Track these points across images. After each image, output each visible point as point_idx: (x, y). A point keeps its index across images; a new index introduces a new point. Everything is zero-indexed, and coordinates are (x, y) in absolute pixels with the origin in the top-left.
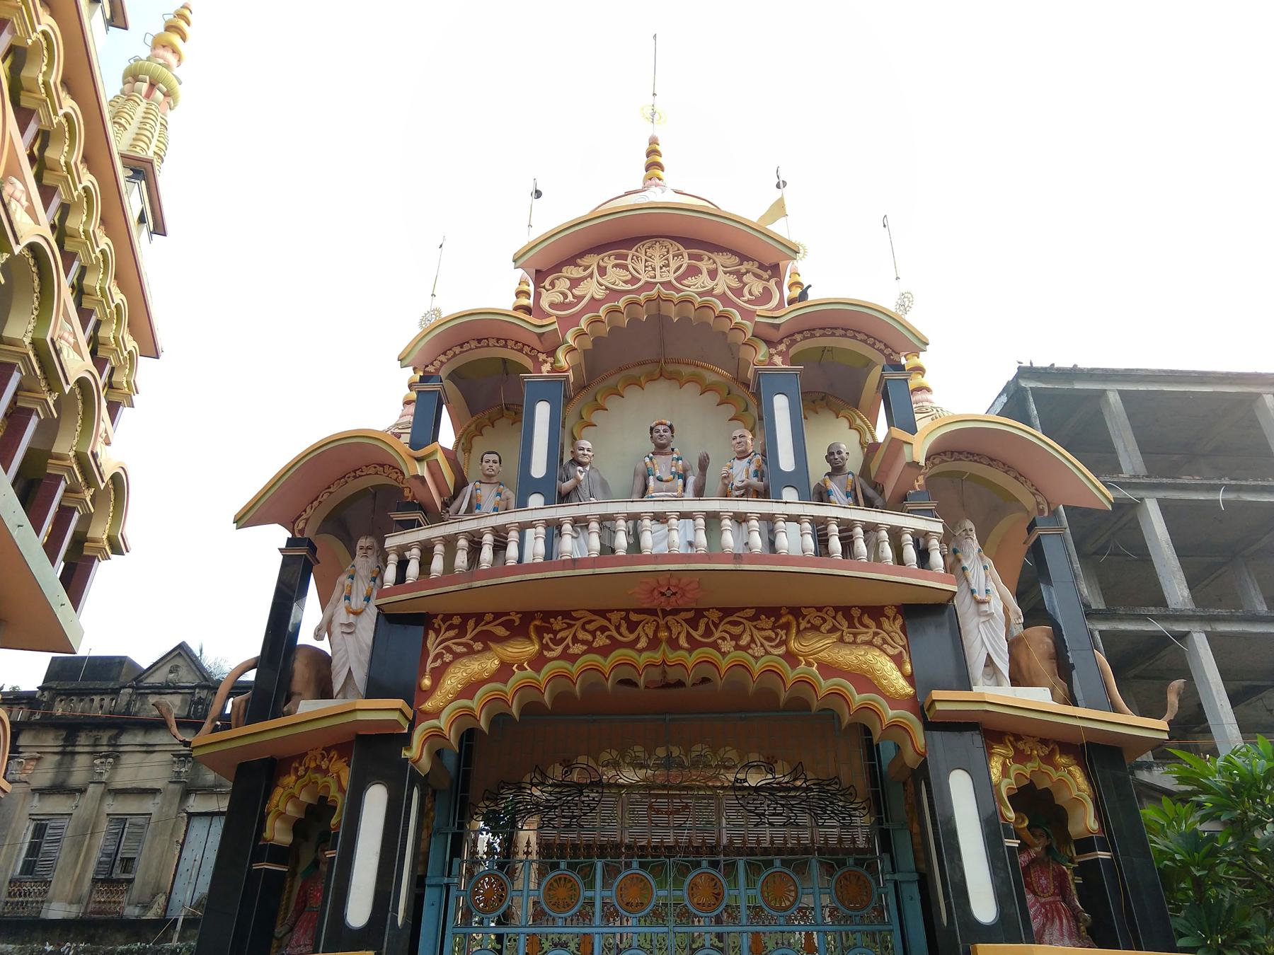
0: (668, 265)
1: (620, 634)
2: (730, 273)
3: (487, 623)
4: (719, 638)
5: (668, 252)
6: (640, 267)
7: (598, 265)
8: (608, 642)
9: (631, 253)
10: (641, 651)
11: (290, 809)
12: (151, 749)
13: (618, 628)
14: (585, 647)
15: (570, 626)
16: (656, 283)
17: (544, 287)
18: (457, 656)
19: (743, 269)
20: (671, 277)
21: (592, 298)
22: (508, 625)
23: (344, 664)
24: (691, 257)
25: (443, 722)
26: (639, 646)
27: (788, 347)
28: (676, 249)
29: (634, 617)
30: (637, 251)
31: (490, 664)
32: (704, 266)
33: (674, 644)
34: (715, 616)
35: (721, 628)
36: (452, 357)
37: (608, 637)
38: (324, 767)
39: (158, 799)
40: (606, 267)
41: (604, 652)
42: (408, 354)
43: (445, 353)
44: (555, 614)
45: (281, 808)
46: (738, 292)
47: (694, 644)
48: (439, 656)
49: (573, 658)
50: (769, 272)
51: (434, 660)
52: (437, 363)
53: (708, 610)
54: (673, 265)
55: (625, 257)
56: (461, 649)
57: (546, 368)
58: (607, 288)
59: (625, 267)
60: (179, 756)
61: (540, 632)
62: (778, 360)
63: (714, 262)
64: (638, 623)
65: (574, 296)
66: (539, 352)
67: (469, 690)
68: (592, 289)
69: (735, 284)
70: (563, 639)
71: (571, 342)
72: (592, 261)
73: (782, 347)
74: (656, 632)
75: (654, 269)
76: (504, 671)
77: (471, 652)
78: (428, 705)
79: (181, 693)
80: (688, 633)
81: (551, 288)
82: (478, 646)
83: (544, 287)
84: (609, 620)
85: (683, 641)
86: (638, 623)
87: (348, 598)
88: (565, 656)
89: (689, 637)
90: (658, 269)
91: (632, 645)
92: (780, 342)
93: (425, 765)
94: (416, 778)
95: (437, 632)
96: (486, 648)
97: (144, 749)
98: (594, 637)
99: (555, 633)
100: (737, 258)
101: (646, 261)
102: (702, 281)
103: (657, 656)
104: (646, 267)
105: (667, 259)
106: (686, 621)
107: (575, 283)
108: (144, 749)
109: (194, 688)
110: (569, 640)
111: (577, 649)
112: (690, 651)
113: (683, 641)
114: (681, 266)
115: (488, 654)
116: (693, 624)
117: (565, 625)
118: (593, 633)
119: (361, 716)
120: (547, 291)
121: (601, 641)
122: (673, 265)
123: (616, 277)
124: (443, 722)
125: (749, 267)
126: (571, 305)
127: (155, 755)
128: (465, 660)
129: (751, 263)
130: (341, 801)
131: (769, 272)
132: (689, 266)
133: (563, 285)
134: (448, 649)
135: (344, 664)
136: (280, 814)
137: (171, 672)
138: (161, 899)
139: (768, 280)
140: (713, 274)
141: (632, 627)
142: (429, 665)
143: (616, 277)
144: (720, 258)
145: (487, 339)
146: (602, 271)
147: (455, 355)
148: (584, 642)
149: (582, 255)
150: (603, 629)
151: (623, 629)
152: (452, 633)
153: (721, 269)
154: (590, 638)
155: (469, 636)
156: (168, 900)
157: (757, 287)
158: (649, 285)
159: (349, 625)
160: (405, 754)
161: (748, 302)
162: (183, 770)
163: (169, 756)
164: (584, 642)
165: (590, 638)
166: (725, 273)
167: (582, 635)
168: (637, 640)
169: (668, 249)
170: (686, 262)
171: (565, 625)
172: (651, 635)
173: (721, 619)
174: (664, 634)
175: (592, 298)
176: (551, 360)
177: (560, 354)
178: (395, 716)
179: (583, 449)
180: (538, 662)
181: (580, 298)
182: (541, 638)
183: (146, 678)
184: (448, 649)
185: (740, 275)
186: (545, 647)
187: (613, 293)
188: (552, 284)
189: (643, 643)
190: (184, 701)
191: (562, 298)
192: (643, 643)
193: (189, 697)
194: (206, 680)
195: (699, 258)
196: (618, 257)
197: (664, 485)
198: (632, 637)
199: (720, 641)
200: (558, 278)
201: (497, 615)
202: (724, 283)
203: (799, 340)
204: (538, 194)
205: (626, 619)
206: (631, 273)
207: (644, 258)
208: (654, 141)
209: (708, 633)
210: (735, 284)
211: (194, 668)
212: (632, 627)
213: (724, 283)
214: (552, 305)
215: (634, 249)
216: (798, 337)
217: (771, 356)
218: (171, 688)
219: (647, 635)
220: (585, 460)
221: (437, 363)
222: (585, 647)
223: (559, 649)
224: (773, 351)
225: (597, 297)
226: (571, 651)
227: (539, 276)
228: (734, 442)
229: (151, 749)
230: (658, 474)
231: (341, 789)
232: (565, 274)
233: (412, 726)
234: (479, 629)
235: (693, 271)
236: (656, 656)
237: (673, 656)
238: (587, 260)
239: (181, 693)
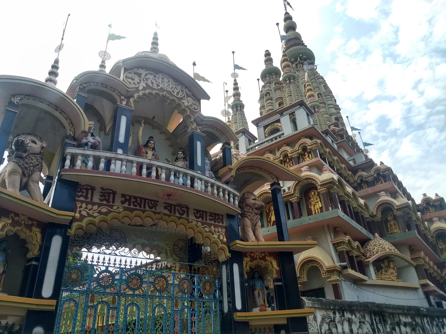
27: (202, 128)
62: (199, 130)
92: (201, 125)
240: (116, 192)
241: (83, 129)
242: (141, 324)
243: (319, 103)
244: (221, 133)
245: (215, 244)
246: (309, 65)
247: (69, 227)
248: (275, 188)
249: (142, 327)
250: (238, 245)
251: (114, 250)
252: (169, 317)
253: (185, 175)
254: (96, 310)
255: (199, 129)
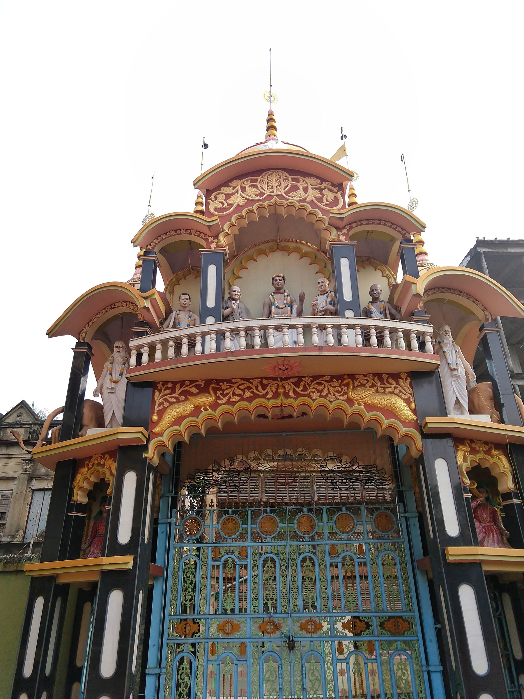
0: (280, 185)
1: (258, 391)
2: (316, 189)
3: (186, 386)
4: (311, 392)
5: (280, 178)
6: (265, 186)
7: (241, 186)
8: (251, 395)
9: (259, 178)
10: (269, 399)
11: (85, 485)
12: (10, 456)
13: (256, 388)
14: (239, 398)
15: (231, 387)
16: (274, 195)
17: (211, 199)
18: (171, 404)
19: (322, 186)
20: (282, 192)
21: (238, 205)
22: (196, 387)
23: (111, 409)
24: (293, 180)
25: (165, 438)
26: (268, 397)
27: (348, 231)
28: (285, 175)
29: (265, 382)
30: (262, 177)
31: (188, 407)
32: (301, 185)
33: (287, 395)
34: (308, 380)
35: (312, 387)
36: (161, 240)
37: (252, 392)
38: (102, 463)
39: (16, 482)
40: (245, 187)
41: (250, 400)
42: (137, 239)
43: (157, 238)
44: (223, 381)
45: (81, 484)
46: (320, 200)
47: (297, 395)
48: (161, 404)
49: (233, 404)
50: (337, 188)
51: (159, 406)
52: (153, 244)
53: (305, 377)
54: (283, 185)
55: (256, 181)
56: (173, 400)
57: (213, 245)
58: (246, 199)
59: (256, 187)
60: (25, 460)
61: (215, 390)
62: (343, 238)
63: (306, 183)
64: (268, 385)
65: (228, 204)
66: (209, 236)
67: (178, 421)
68: (238, 200)
69: (318, 195)
70: (227, 394)
71: (227, 230)
72: (238, 183)
73: (345, 231)
74: (277, 389)
75: (272, 188)
76: (197, 411)
77: (178, 401)
78: (156, 430)
79: (24, 427)
80: (294, 389)
81: (214, 199)
82: (182, 398)
83: (211, 199)
84: (252, 384)
85: (291, 394)
86: (268, 385)
87: (110, 374)
88: (229, 402)
89: (295, 392)
90: (275, 187)
91: (264, 396)
92: (344, 228)
93: (156, 461)
94: (151, 468)
95: (160, 391)
96: (187, 399)
97: (7, 456)
98: (244, 393)
99: (223, 391)
100: (319, 180)
101: (268, 183)
102: (300, 194)
103: (278, 402)
104: (268, 186)
105: (280, 182)
106: (293, 383)
107: (228, 196)
108: (7, 456)
109: (31, 424)
110: (231, 394)
111: (235, 399)
112: (296, 399)
113: (291, 394)
114: (288, 185)
115: (187, 402)
116: (297, 384)
117: (228, 387)
118: (243, 391)
119: (120, 436)
120: (213, 201)
121: (248, 394)
122: (283, 185)
123: (251, 193)
124: (165, 438)
125: (326, 185)
126: (226, 209)
127: (13, 459)
128: (175, 406)
129: (327, 183)
130: (112, 480)
131: (337, 188)
132: (292, 186)
133: (221, 198)
134: (166, 400)
135: (111, 409)
136: (81, 488)
137: (18, 416)
138: (21, 533)
139: (336, 193)
140: (306, 190)
141: (264, 387)
142: (156, 409)
143: (251, 193)
144: (310, 181)
145: (180, 230)
146: (243, 189)
147: (163, 239)
148: (238, 395)
149: (231, 180)
150: (249, 388)
151: (260, 388)
152: (168, 392)
153: (310, 187)
154: (242, 393)
155: (177, 393)
156: (25, 533)
157: (331, 197)
158: (270, 197)
159: (112, 388)
160: (145, 455)
161: (326, 205)
162: (28, 467)
163: (20, 460)
164: (238, 395)
165: (242, 393)
166: (313, 189)
167: (237, 392)
168: (267, 393)
169: (280, 176)
170: (290, 183)
171: (228, 387)
172: (274, 391)
173: (312, 382)
174: (281, 390)
175: (238, 205)
176: (216, 241)
177: (221, 237)
178: (139, 436)
179: (235, 291)
180: (214, 406)
181: (231, 205)
182: (216, 393)
183: (5, 419)
184: (166, 400)
185: (321, 190)
186: (218, 398)
187: (250, 202)
188: (216, 198)
189: (270, 395)
190: (26, 431)
191: (221, 205)
192: (270, 395)
193: (28, 429)
194: (37, 420)
195: (298, 181)
196: (252, 181)
197: (280, 311)
198: (264, 392)
199: (311, 393)
200: (218, 194)
201: (192, 382)
202: (312, 194)
203: (354, 226)
204: (206, 146)
205: (261, 383)
206: (259, 190)
207: (267, 181)
208: (271, 114)
209: (305, 389)
210: (318, 195)
211: (30, 414)
212: (264, 387)
213: (312, 194)
214: (216, 209)
215: (261, 176)
216: (354, 225)
217: (339, 236)
218: (19, 425)
219: (272, 391)
220: (237, 297)
221: (153, 244)
222: (239, 398)
223: (225, 399)
224: (340, 233)
225: (241, 204)
226: (232, 400)
227: (208, 193)
228: (319, 285)
229: (10, 456)
230: (277, 305)
231: (112, 474)
232: (222, 192)
233: (148, 441)
234: (182, 389)
235: (295, 188)
236: (278, 402)
237: (286, 402)
238: (234, 183)
239: (24, 427)
240: (469, 414)
241: (414, 293)
242: (283, 604)
243: (258, 188)
244: (379, 222)
245: (408, 438)
246: (145, 219)
247: (145, 448)
248: (145, 331)
249: (286, 608)
250: (430, 425)
251: (237, 486)
252: (285, 570)
253: (322, 328)
254: (348, 663)
255: (344, 234)
